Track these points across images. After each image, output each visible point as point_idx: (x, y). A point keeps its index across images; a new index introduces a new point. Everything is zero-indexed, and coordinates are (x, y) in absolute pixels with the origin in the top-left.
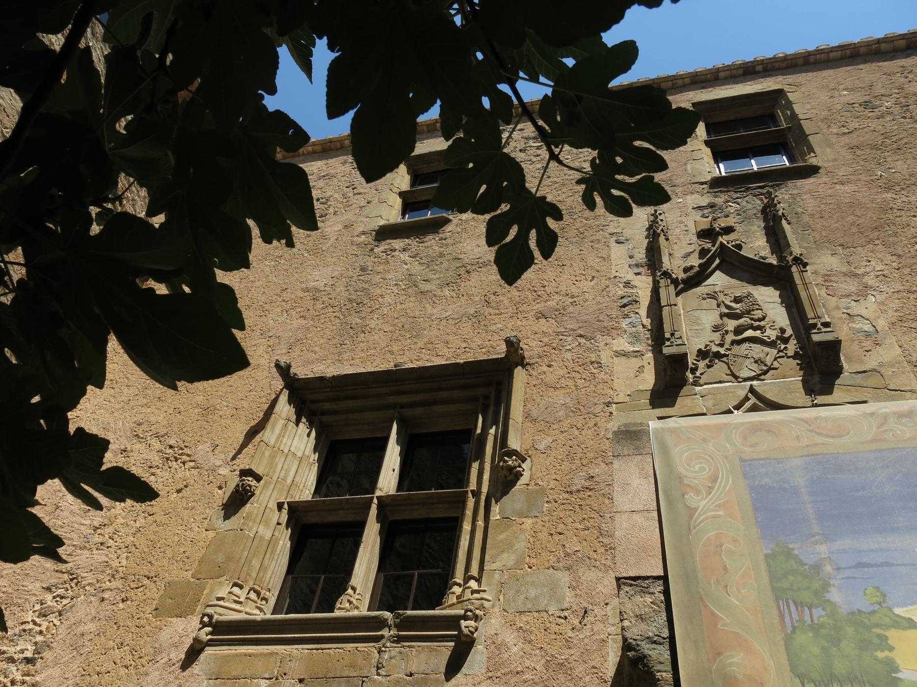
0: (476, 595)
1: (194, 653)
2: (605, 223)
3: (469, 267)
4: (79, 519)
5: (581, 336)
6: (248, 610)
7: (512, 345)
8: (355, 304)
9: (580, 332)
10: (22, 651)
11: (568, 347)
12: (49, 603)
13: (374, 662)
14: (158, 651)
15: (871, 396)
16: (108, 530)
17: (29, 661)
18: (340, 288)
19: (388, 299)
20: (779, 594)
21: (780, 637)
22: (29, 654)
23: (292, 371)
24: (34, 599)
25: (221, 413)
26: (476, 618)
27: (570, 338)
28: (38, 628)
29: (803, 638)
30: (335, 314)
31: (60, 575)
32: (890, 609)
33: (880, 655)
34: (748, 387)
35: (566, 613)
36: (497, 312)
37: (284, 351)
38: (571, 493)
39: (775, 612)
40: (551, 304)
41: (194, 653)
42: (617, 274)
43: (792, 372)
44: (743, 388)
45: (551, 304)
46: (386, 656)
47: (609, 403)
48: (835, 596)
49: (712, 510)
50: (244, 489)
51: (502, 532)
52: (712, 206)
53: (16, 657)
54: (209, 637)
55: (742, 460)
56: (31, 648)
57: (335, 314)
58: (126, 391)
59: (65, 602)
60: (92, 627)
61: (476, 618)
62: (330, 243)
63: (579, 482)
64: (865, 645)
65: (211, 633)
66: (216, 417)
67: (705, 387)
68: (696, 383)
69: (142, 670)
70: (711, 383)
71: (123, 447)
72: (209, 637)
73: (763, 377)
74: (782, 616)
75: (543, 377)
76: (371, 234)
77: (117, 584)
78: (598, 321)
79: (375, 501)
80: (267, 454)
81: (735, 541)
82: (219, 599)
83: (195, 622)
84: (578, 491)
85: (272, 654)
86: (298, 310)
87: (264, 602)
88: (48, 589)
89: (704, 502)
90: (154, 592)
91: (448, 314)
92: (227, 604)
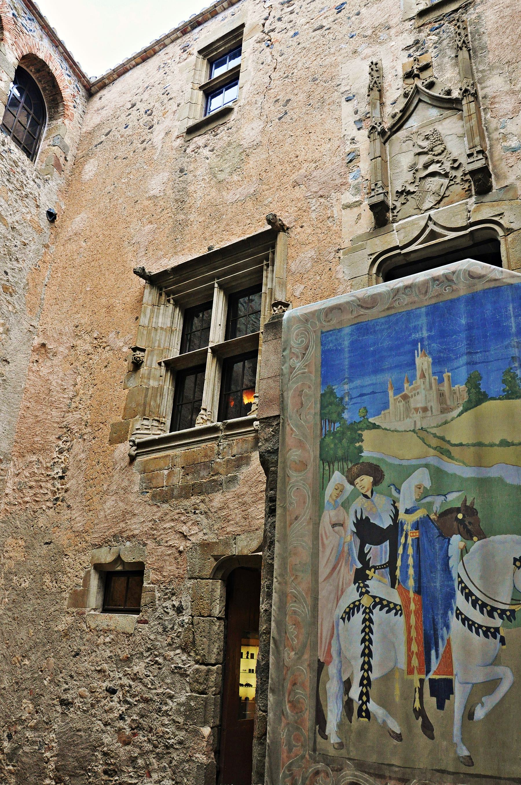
1: (132, 459)
2: (339, 83)
3: (248, 151)
4: (62, 395)
5: (321, 196)
6: (154, 432)
7: (272, 220)
8: (179, 203)
9: (321, 193)
10: (57, 473)
11: (314, 208)
12: (62, 446)
13: (216, 451)
14: (115, 463)
15: (506, 207)
16: (78, 398)
17: (62, 478)
18: (169, 192)
19: (199, 194)
22: (60, 474)
23: (147, 271)
24: (54, 445)
25: (117, 309)
27: (314, 200)
28: (60, 460)
30: (169, 215)
31: (61, 429)
32: (367, 419)
34: (427, 217)
36: (267, 187)
37: (143, 253)
39: (319, 427)
40: (302, 171)
41: (132, 459)
42: (346, 133)
44: (423, 218)
45: (302, 171)
46: (221, 448)
47: (339, 250)
49: (303, 369)
50: (136, 360)
52: (417, 42)
53: (55, 476)
54: (136, 452)
55: (322, 333)
56: (60, 471)
57: (169, 215)
58: (65, 305)
59: (68, 444)
60: (83, 456)
62: (158, 151)
64: (353, 441)
65: (136, 450)
66: (114, 312)
67: (400, 222)
68: (394, 221)
69: (111, 474)
70: (404, 219)
71: (72, 345)
72: (136, 452)
73: (437, 207)
74: (322, 429)
75: (298, 237)
76: (183, 136)
77: (89, 429)
78: (333, 180)
79: (209, 350)
80: (145, 332)
81: (310, 387)
82: (137, 429)
83: (128, 444)
85: (167, 456)
86: (147, 217)
87: (162, 425)
88: (59, 438)
89: (299, 364)
90: (107, 431)
91: (237, 197)
92: (142, 432)
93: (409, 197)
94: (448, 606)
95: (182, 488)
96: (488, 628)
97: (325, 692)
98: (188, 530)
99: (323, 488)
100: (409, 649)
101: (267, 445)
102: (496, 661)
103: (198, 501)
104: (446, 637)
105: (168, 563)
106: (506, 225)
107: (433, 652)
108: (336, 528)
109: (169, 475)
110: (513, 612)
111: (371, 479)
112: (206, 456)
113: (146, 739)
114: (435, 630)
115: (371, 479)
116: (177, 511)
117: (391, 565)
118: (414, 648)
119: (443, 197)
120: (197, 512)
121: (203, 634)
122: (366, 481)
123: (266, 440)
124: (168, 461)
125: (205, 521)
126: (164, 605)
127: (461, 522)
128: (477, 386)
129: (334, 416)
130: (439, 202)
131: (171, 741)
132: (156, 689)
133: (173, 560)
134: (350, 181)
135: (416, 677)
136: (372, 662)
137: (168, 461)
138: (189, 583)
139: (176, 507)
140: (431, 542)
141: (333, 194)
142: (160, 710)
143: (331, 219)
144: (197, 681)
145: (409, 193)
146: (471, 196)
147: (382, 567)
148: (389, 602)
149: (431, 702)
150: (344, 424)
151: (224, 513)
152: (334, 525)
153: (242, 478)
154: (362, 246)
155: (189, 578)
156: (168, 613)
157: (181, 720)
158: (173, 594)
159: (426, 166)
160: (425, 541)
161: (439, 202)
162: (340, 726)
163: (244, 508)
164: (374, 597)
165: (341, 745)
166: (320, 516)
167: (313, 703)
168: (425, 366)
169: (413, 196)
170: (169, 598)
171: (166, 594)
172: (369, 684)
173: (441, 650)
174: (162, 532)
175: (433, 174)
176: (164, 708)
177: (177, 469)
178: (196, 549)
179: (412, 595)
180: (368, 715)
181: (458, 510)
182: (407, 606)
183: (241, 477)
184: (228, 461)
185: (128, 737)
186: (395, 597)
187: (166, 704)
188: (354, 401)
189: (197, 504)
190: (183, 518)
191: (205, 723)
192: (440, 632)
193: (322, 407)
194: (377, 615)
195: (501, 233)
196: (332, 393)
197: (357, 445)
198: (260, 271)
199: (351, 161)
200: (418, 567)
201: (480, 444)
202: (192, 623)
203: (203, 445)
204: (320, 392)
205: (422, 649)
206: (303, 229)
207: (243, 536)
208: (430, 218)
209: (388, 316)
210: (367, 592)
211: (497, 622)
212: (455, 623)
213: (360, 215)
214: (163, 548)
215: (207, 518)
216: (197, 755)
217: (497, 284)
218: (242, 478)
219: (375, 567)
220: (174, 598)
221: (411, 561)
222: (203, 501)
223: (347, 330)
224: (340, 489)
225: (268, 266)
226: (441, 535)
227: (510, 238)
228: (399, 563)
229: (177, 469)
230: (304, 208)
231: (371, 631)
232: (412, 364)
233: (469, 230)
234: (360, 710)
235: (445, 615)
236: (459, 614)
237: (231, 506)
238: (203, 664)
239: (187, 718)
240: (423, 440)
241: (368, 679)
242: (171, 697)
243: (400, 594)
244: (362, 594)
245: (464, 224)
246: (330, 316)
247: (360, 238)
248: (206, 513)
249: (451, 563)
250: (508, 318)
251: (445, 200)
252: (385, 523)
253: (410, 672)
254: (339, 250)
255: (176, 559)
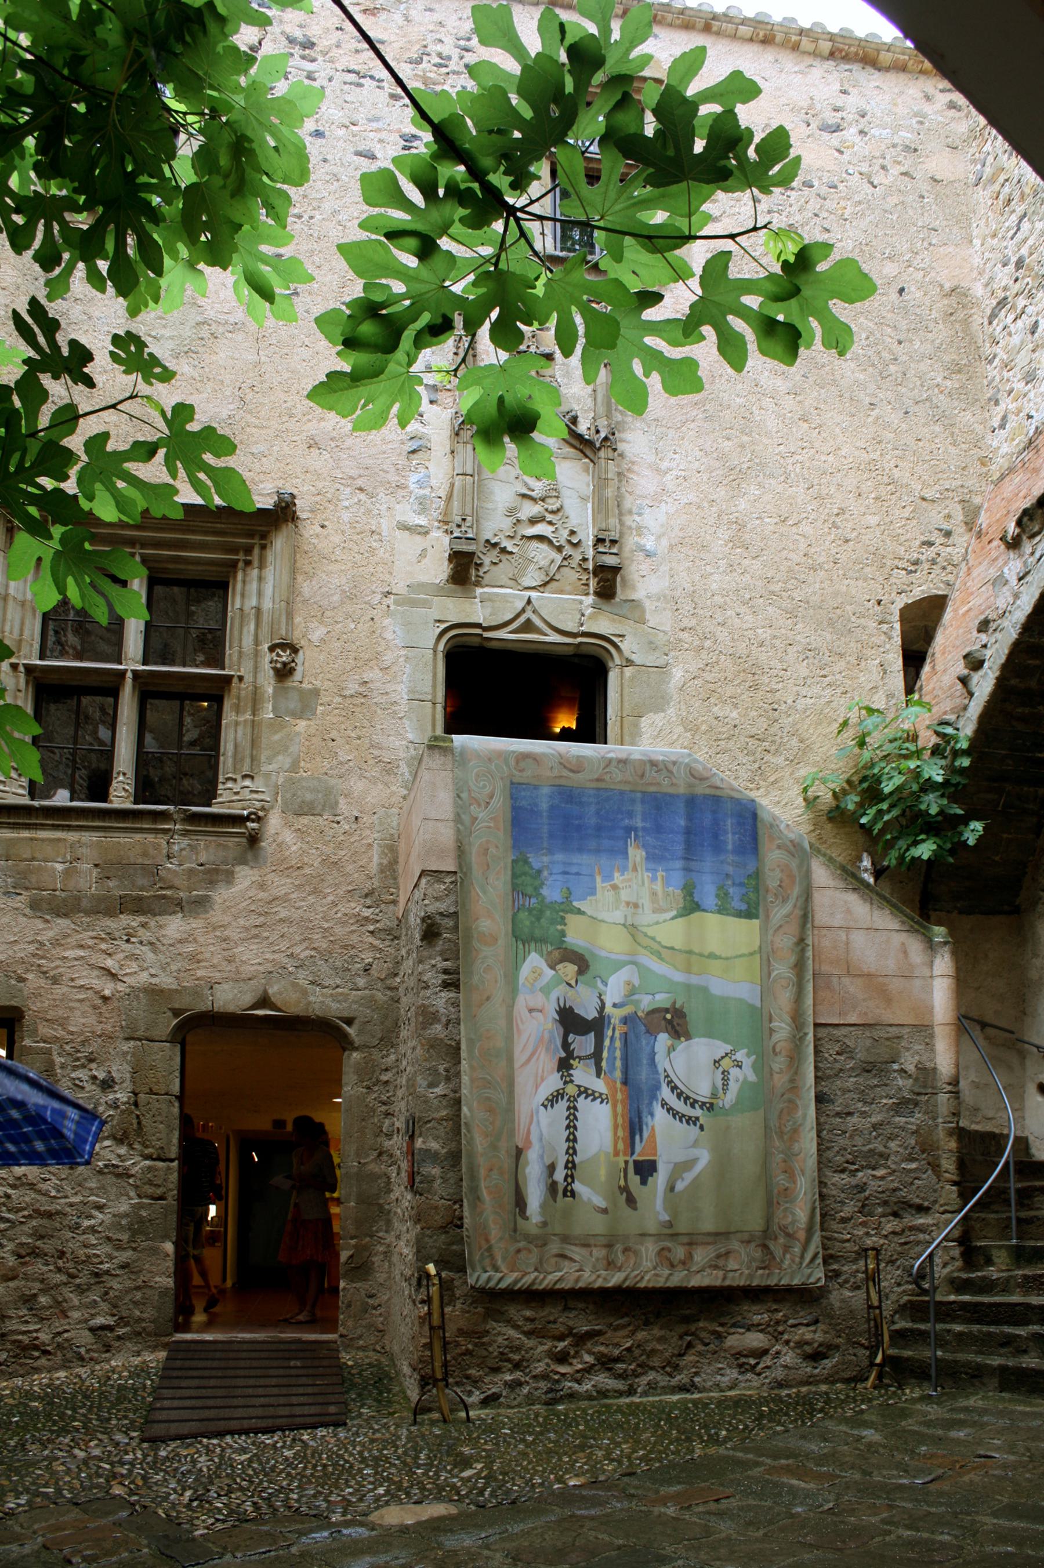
0: (255, 796)
5: (361, 489)
9: (360, 483)
11: (346, 503)
20: (515, 888)
21: (510, 914)
26: (259, 819)
27: (348, 490)
29: (523, 915)
33: (559, 927)
35: (338, 818)
38: (345, 697)
43: (568, 588)
47: (389, 593)
48: (545, 891)
51: (276, 732)
55: (512, 783)
61: (259, 819)
63: (353, 688)
79: (129, 675)
84: (352, 696)
85: (59, 840)
93: (504, 557)
94: (653, 1097)
95: (100, 899)
96: (690, 1118)
97: (525, 1177)
98: (117, 966)
99: (517, 968)
100: (615, 1133)
101: (438, 904)
102: (695, 1144)
103: (134, 924)
104: (650, 1124)
105: (78, 1013)
106: (627, 653)
107: (637, 1137)
108: (534, 1014)
109: (67, 872)
110: (712, 1104)
111: (576, 968)
112: (145, 854)
113: (51, 1267)
114: (640, 1118)
115: (576, 968)
116: (94, 934)
117: (597, 1056)
118: (620, 1133)
119: (552, 579)
120: (133, 940)
121: (159, 1118)
122: (571, 969)
123: (437, 899)
124: (63, 851)
125: (150, 956)
126: (73, 1075)
127: (670, 1022)
128: (691, 894)
129: (529, 890)
130: (545, 584)
131: (105, 1266)
132: (66, 1197)
133: (90, 1010)
134: (412, 486)
135: (621, 1159)
136: (577, 1147)
137: (63, 851)
138: (126, 1046)
139: (89, 927)
140: (637, 1037)
141: (382, 495)
142: (78, 1226)
143: (376, 537)
144: (150, 1183)
145: (504, 550)
146: (587, 594)
147: (587, 1057)
148: (594, 1092)
149: (634, 1180)
150: (543, 901)
151: (190, 948)
152: (531, 1011)
153: (220, 901)
154: (425, 601)
155: (127, 1039)
156: (83, 1088)
157: (125, 1237)
158: (92, 1061)
159: (533, 521)
160: (631, 1037)
161: (545, 584)
162: (543, 1206)
163: (225, 946)
164: (579, 1086)
165: (545, 1224)
166: (513, 999)
167: (513, 1188)
168: (638, 859)
169: (509, 557)
170: (83, 1066)
171: (78, 1059)
172: (574, 1166)
173: (646, 1134)
174: (58, 963)
175: (540, 538)
176: (86, 1223)
177: (85, 866)
178: (138, 997)
179: (619, 1085)
180: (573, 1194)
181: (667, 1011)
182: (614, 1095)
183: (218, 899)
184: (191, 871)
185: (12, 1269)
186: (599, 1086)
187: (90, 1217)
188: (554, 877)
189: (133, 928)
190: (104, 946)
191: (165, 1237)
192: (644, 1119)
193: (514, 876)
194: (582, 1103)
195: (618, 661)
196: (526, 862)
197: (559, 927)
198: (233, 565)
199: (414, 452)
200: (625, 1059)
201: (690, 952)
202: (136, 1104)
203: (138, 837)
204: (511, 857)
205: (627, 1134)
206: (325, 532)
207: (225, 986)
208: (529, 602)
209: (598, 789)
210: (572, 1081)
211: (697, 1112)
212: (659, 1112)
213: (424, 550)
214: (65, 989)
215: (155, 951)
216: (157, 1279)
217: (718, 793)
218: (220, 901)
219: (580, 1058)
220: (93, 1066)
221: (618, 1054)
222: (143, 925)
223: (545, 790)
224: (537, 973)
225: (248, 563)
226: (648, 1032)
227: (628, 671)
228: (605, 1054)
229: (85, 866)
230: (329, 495)
231: (576, 1118)
232: (625, 853)
233: (580, 640)
234: (565, 1191)
235: (650, 1104)
236: (664, 1104)
237: (201, 939)
238: (159, 1159)
239: (134, 1233)
240: (633, 936)
241: (573, 1162)
242: (100, 1208)
243: (607, 1084)
244: (566, 1083)
245: (575, 631)
246: (522, 764)
247: (421, 587)
248: (151, 944)
249: (657, 1058)
250: (726, 832)
251: (553, 584)
252: (591, 1014)
253: (616, 1154)
254: (389, 593)
255: (95, 1007)
